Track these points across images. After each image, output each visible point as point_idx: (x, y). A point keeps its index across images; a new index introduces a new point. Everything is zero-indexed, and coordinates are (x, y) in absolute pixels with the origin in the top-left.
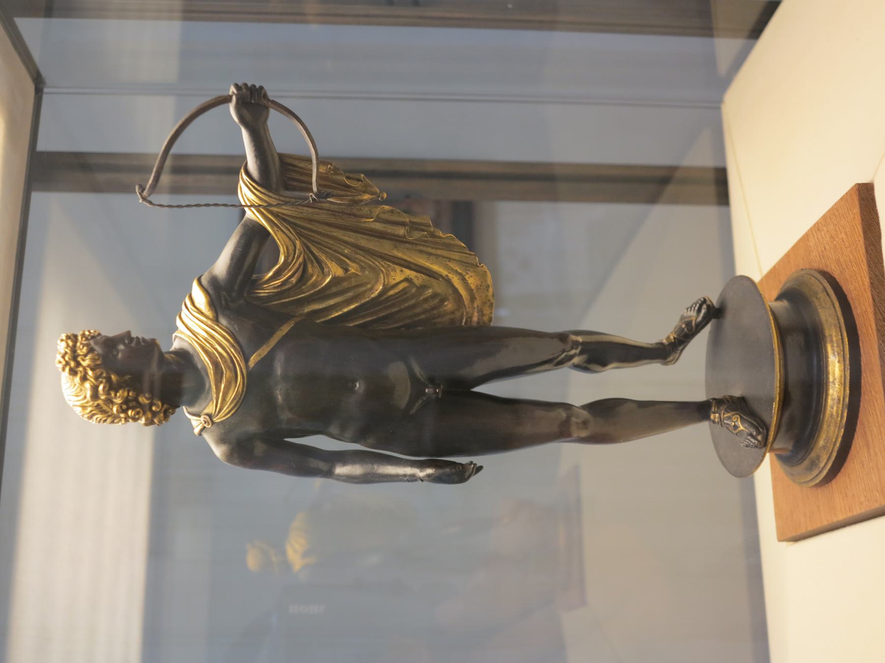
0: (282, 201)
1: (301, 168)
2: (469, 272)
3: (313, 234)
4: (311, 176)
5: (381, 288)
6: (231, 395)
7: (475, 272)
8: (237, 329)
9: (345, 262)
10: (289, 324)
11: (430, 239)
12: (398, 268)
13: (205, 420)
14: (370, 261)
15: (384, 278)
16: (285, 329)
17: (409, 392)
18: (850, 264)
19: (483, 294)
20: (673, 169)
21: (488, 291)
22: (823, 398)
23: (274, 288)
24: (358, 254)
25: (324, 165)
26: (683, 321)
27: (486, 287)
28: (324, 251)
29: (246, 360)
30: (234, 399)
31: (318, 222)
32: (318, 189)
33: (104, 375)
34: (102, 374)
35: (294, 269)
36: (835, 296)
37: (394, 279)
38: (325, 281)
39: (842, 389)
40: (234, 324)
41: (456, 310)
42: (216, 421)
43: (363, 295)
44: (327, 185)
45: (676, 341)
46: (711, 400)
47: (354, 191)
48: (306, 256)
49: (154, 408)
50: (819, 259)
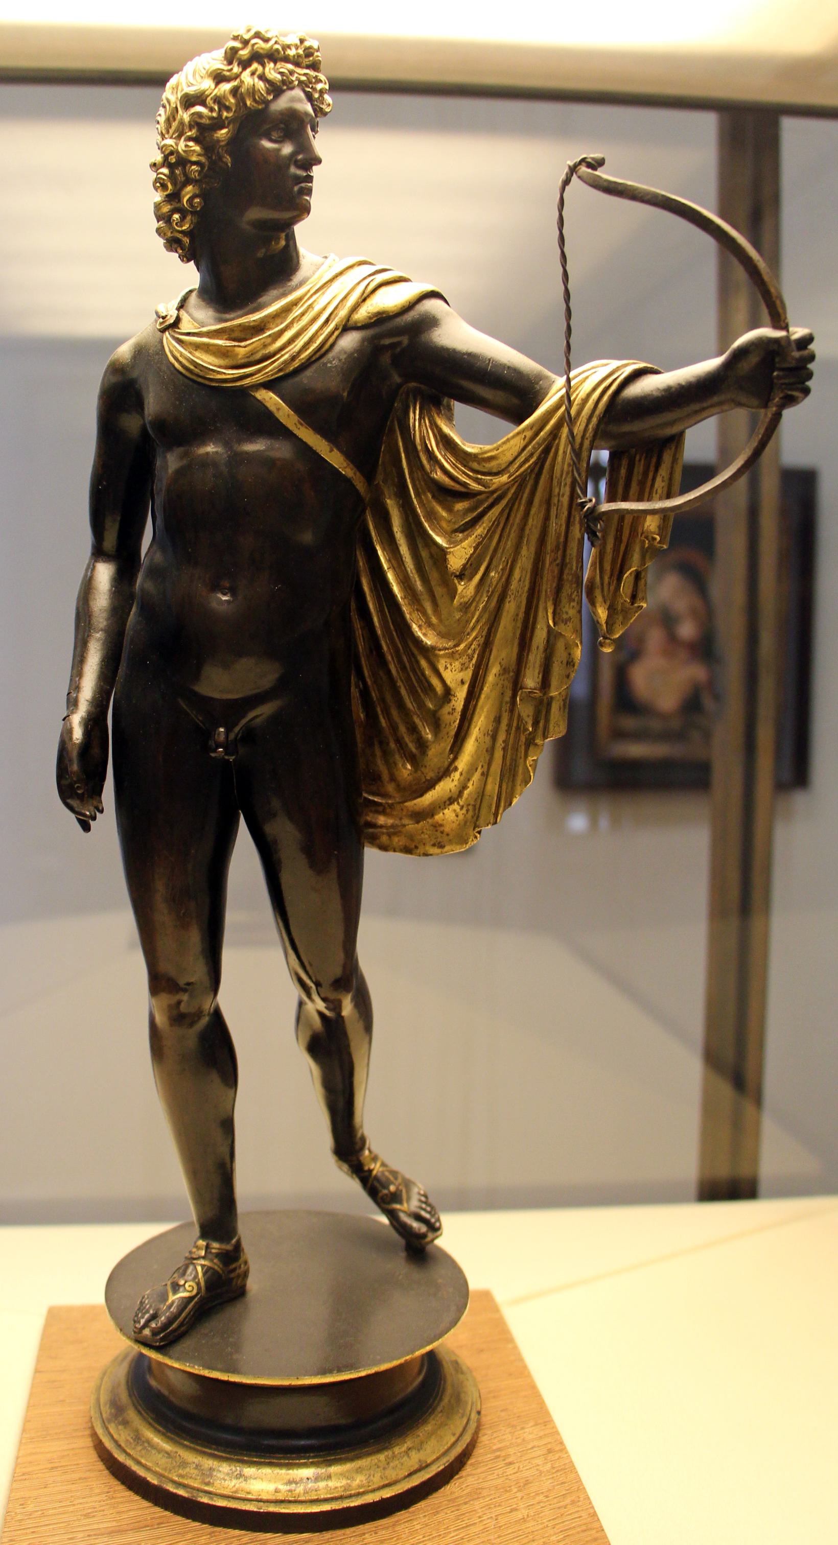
0: (581, 444)
1: (654, 479)
2: (464, 811)
3: (522, 508)
4: (640, 499)
5: (429, 643)
6: (206, 360)
7: (466, 822)
8: (329, 365)
9: (476, 573)
10: (345, 464)
11: (523, 739)
12: (468, 675)
13: (168, 317)
14: (478, 621)
15: (446, 649)
16: (335, 459)
17: (216, 695)
18: (464, 1524)
19: (426, 836)
20: (758, 1100)
21: (434, 845)
22: (218, 1451)
23: (423, 439)
24: (489, 598)
25: (659, 527)
26: (400, 1187)
27: (439, 843)
28: (494, 532)
29: (269, 385)
30: (196, 365)
31: (547, 518)
32: (604, 513)
33: (225, 114)
34: (228, 109)
35: (456, 474)
36: (405, 1489)
37: (446, 668)
38: (438, 535)
39: (225, 1492)
40: (340, 360)
41: (398, 785)
42: (164, 336)
43: (417, 610)
44: (621, 535)
45: (366, 1174)
46: (234, 1241)
47: (612, 588)
48: (483, 496)
49: (176, 216)
50: (494, 1447)
